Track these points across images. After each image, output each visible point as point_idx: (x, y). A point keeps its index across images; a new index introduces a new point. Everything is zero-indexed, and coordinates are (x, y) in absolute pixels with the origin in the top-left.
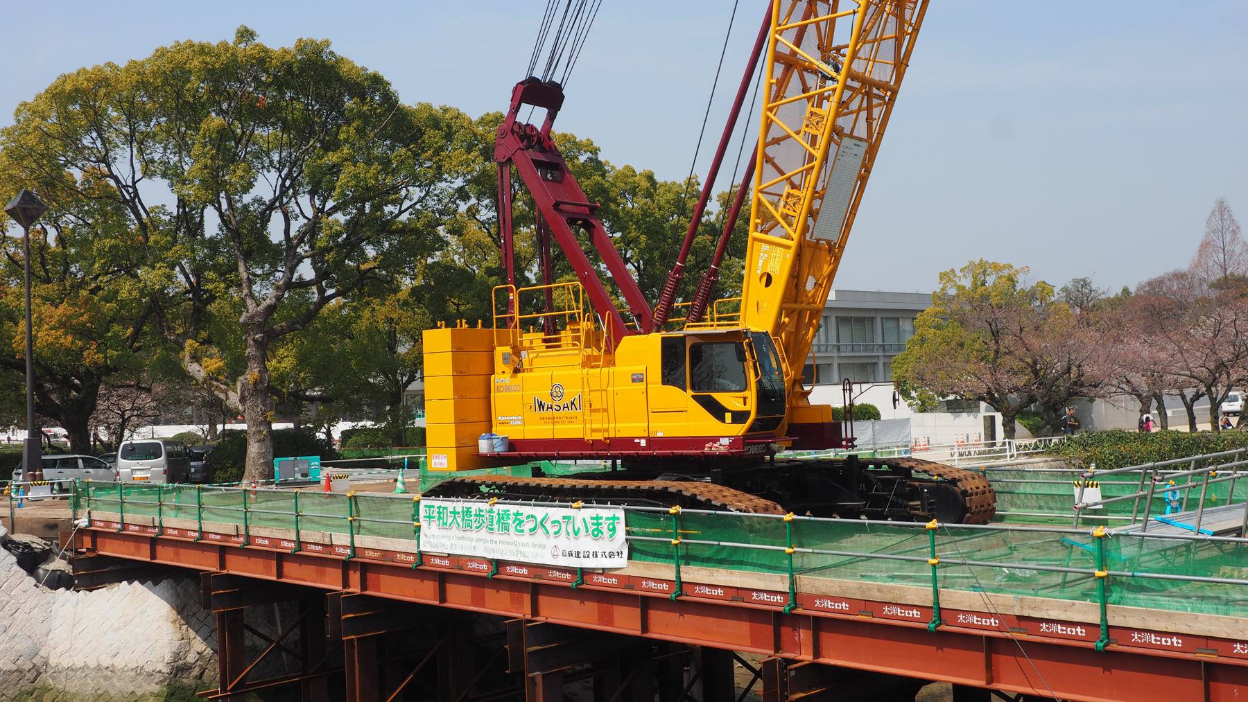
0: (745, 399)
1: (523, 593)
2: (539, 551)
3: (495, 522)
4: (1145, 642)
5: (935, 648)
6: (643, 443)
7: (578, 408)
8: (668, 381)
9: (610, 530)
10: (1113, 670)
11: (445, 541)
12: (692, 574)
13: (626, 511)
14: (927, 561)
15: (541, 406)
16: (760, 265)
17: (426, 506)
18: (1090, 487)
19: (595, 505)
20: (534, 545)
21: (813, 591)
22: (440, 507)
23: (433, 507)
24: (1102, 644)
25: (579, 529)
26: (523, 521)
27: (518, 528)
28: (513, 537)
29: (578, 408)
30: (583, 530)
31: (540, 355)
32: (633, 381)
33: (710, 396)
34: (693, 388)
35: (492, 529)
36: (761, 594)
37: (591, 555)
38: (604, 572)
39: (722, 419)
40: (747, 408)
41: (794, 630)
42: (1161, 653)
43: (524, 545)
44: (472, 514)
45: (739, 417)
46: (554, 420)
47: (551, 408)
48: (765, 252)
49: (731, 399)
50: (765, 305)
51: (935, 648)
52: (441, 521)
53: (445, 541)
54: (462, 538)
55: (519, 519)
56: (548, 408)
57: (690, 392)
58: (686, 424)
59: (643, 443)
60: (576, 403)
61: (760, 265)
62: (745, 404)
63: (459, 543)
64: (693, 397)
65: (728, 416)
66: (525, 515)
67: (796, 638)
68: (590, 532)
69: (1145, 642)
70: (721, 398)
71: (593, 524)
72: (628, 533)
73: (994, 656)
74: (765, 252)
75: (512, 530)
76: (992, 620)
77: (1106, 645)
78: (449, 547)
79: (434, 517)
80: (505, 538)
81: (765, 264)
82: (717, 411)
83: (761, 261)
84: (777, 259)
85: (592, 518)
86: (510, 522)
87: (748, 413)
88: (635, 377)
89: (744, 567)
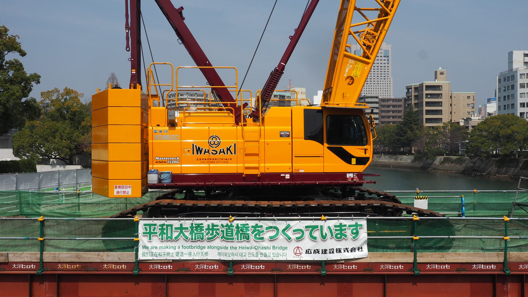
0: (365, 150)
1: (260, 283)
2: (281, 252)
3: (234, 234)
4: (109, 268)
5: (39, 283)
6: (288, 176)
7: (233, 152)
8: (362, 137)
9: (353, 233)
10: (139, 283)
11: (171, 251)
12: (424, 257)
13: (368, 220)
14: (38, 239)
15: (199, 150)
16: (347, 71)
17: (145, 225)
18: (423, 199)
19: (166, 218)
20: (274, 248)
21: (519, 261)
22: (162, 225)
23: (155, 225)
24: (40, 271)
25: (326, 234)
26: (263, 231)
27: (257, 236)
28: (253, 243)
29: (233, 152)
30: (329, 235)
31: (191, 114)
32: (281, 136)
33: (341, 147)
34: (328, 143)
35: (233, 239)
36: (480, 265)
37: (335, 252)
38: (347, 262)
39: (350, 162)
40: (367, 155)
41: (504, 284)
42: (254, 273)
43: (265, 248)
44: (204, 228)
45: (361, 161)
46: (210, 161)
47: (208, 152)
48: (351, 64)
49: (356, 150)
50: (348, 95)
51: (39, 283)
52: (165, 236)
53: (171, 251)
54: (191, 247)
55: (258, 230)
56: (205, 152)
57: (326, 145)
58: (235, 165)
59: (288, 176)
60: (232, 149)
61: (347, 71)
62: (365, 153)
63: (186, 251)
64: (328, 148)
65: (354, 161)
66: (265, 226)
67: (505, 289)
68: (334, 236)
69: (109, 268)
70: (350, 149)
71: (336, 230)
72: (369, 234)
73: (168, 283)
74: (351, 64)
75: (252, 237)
76: (308, 266)
77: (42, 271)
78: (174, 255)
79: (156, 233)
80: (245, 244)
81: (350, 71)
82: (346, 157)
83: (347, 69)
84: (359, 69)
85: (336, 226)
86: (249, 232)
87: (368, 159)
88: (283, 133)
89: (385, 250)
